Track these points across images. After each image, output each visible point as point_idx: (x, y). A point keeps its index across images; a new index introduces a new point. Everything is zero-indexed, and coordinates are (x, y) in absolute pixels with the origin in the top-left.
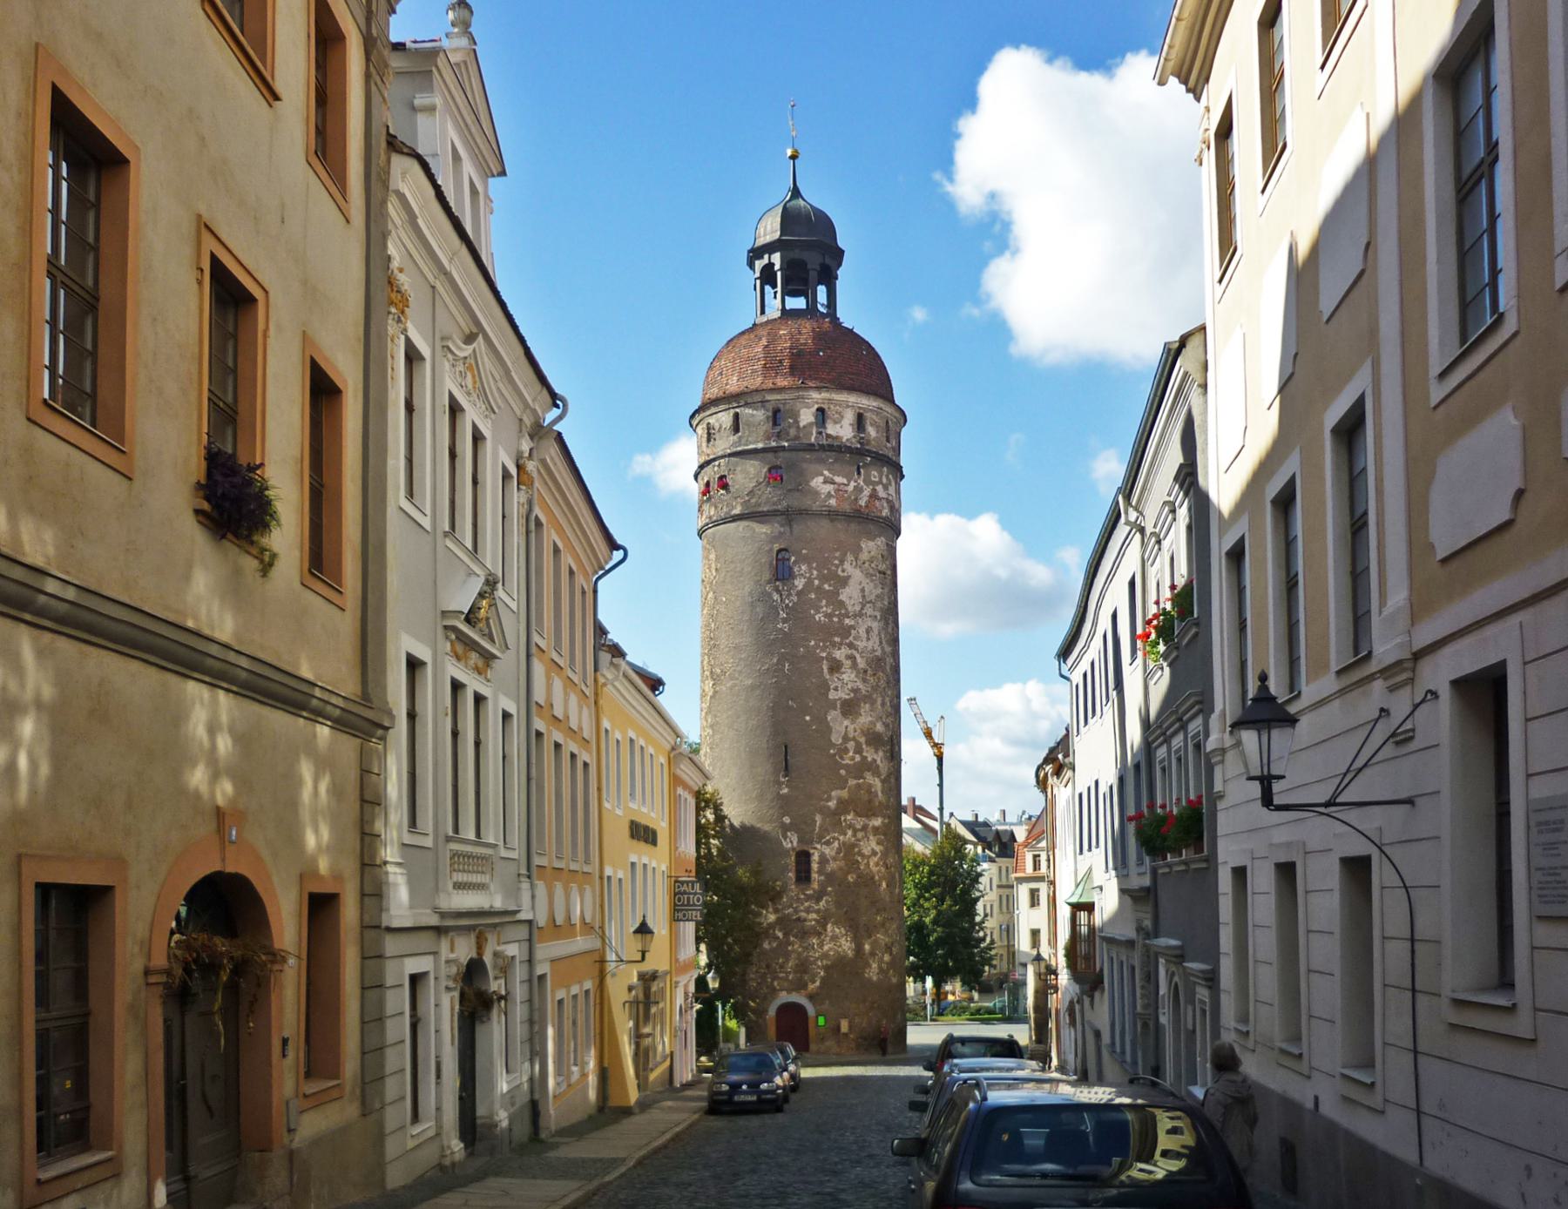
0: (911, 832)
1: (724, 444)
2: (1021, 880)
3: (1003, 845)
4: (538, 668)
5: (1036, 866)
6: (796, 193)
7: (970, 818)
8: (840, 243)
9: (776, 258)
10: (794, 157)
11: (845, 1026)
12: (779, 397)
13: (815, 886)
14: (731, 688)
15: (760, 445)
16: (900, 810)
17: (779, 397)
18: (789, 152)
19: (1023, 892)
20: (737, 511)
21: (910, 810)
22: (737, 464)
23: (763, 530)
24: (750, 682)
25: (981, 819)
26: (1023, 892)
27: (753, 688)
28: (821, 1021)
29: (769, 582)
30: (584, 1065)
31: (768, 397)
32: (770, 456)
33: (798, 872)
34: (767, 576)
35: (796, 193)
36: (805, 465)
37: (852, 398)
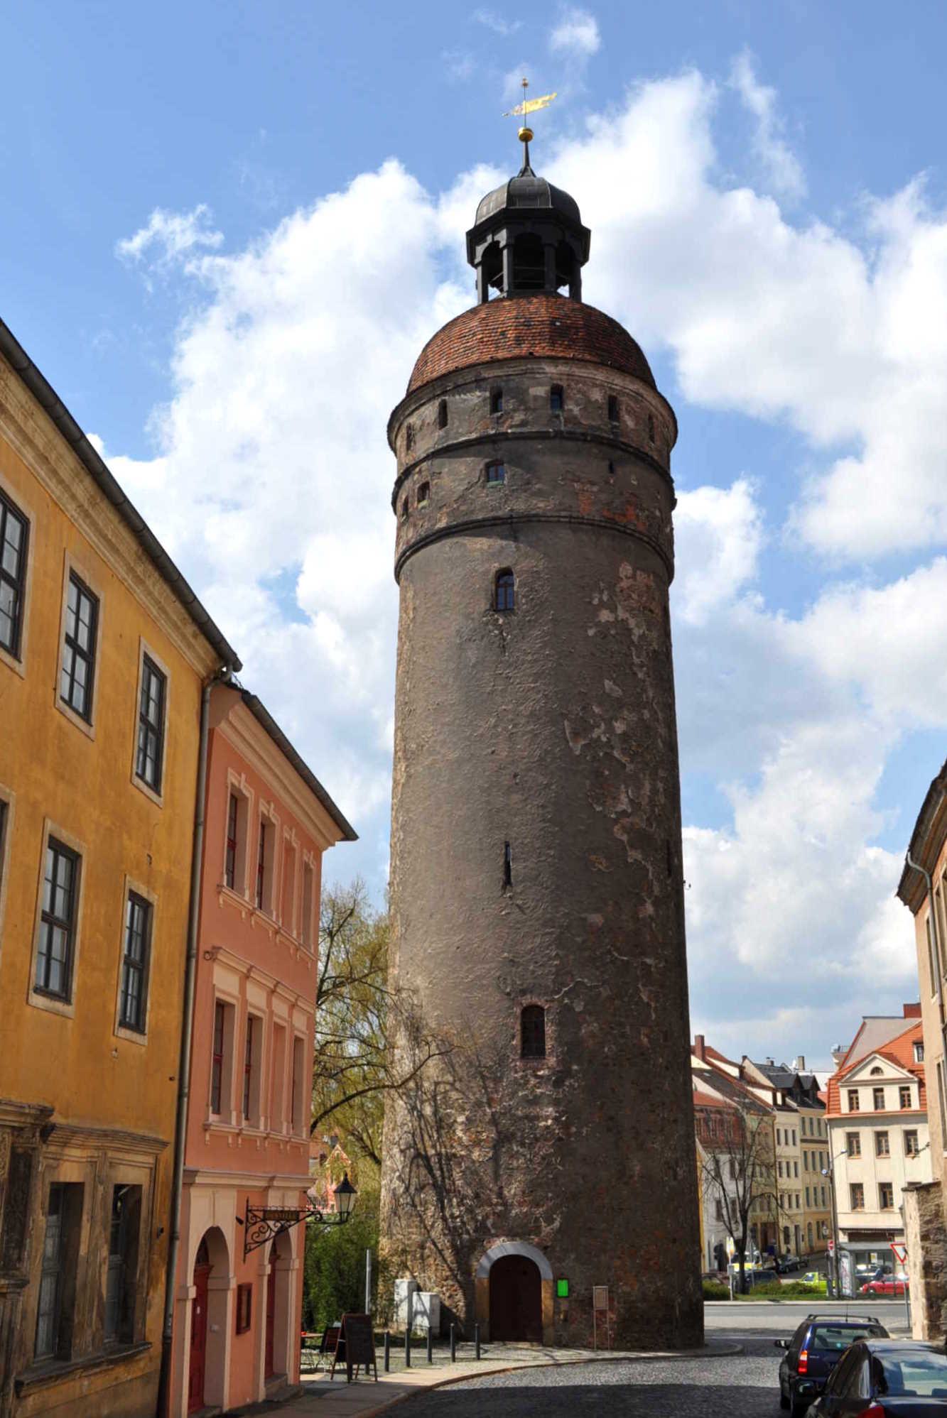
0: (700, 1073)
1: (424, 446)
2: (834, 1123)
3: (801, 1092)
4: (83, 641)
5: (854, 1102)
6: (526, 170)
7: (764, 1062)
8: (586, 221)
9: (502, 237)
10: (526, 137)
11: (600, 1295)
12: (498, 372)
13: (552, 1061)
14: (429, 767)
15: (474, 436)
16: (689, 1051)
17: (498, 372)
18: (521, 131)
19: (838, 1138)
20: (442, 524)
21: (699, 1052)
22: (442, 465)
23: (479, 544)
24: (453, 756)
25: (777, 1064)
26: (838, 1138)
27: (459, 762)
28: (563, 1288)
29: (485, 614)
30: (555, 1296)
31: (485, 375)
32: (488, 448)
33: (525, 1041)
34: (483, 605)
35: (526, 170)
36: (536, 458)
37: (600, 376)
